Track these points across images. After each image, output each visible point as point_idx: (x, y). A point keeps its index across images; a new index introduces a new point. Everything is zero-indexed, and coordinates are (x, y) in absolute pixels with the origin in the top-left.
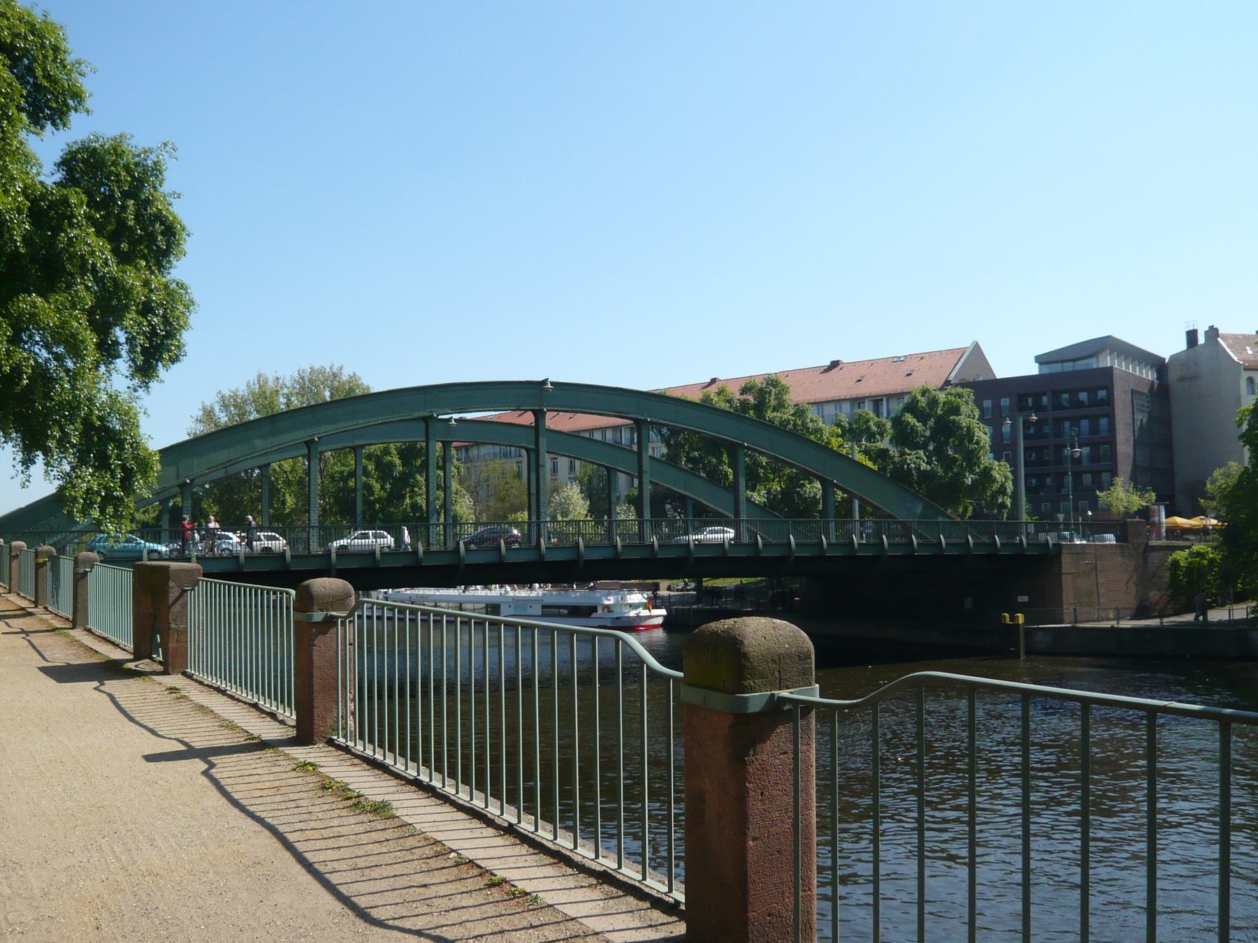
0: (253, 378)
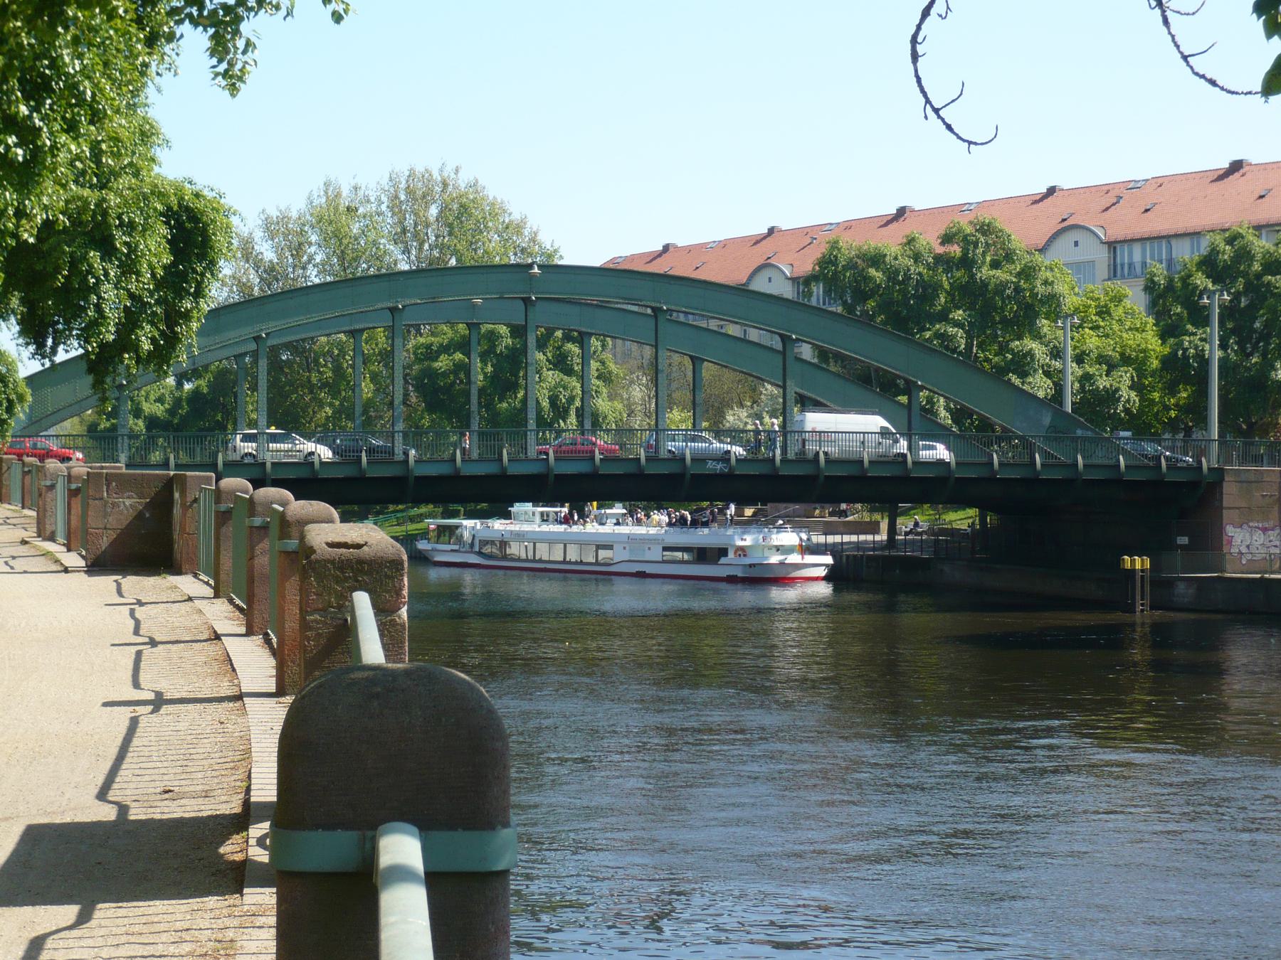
0: (316, 186)
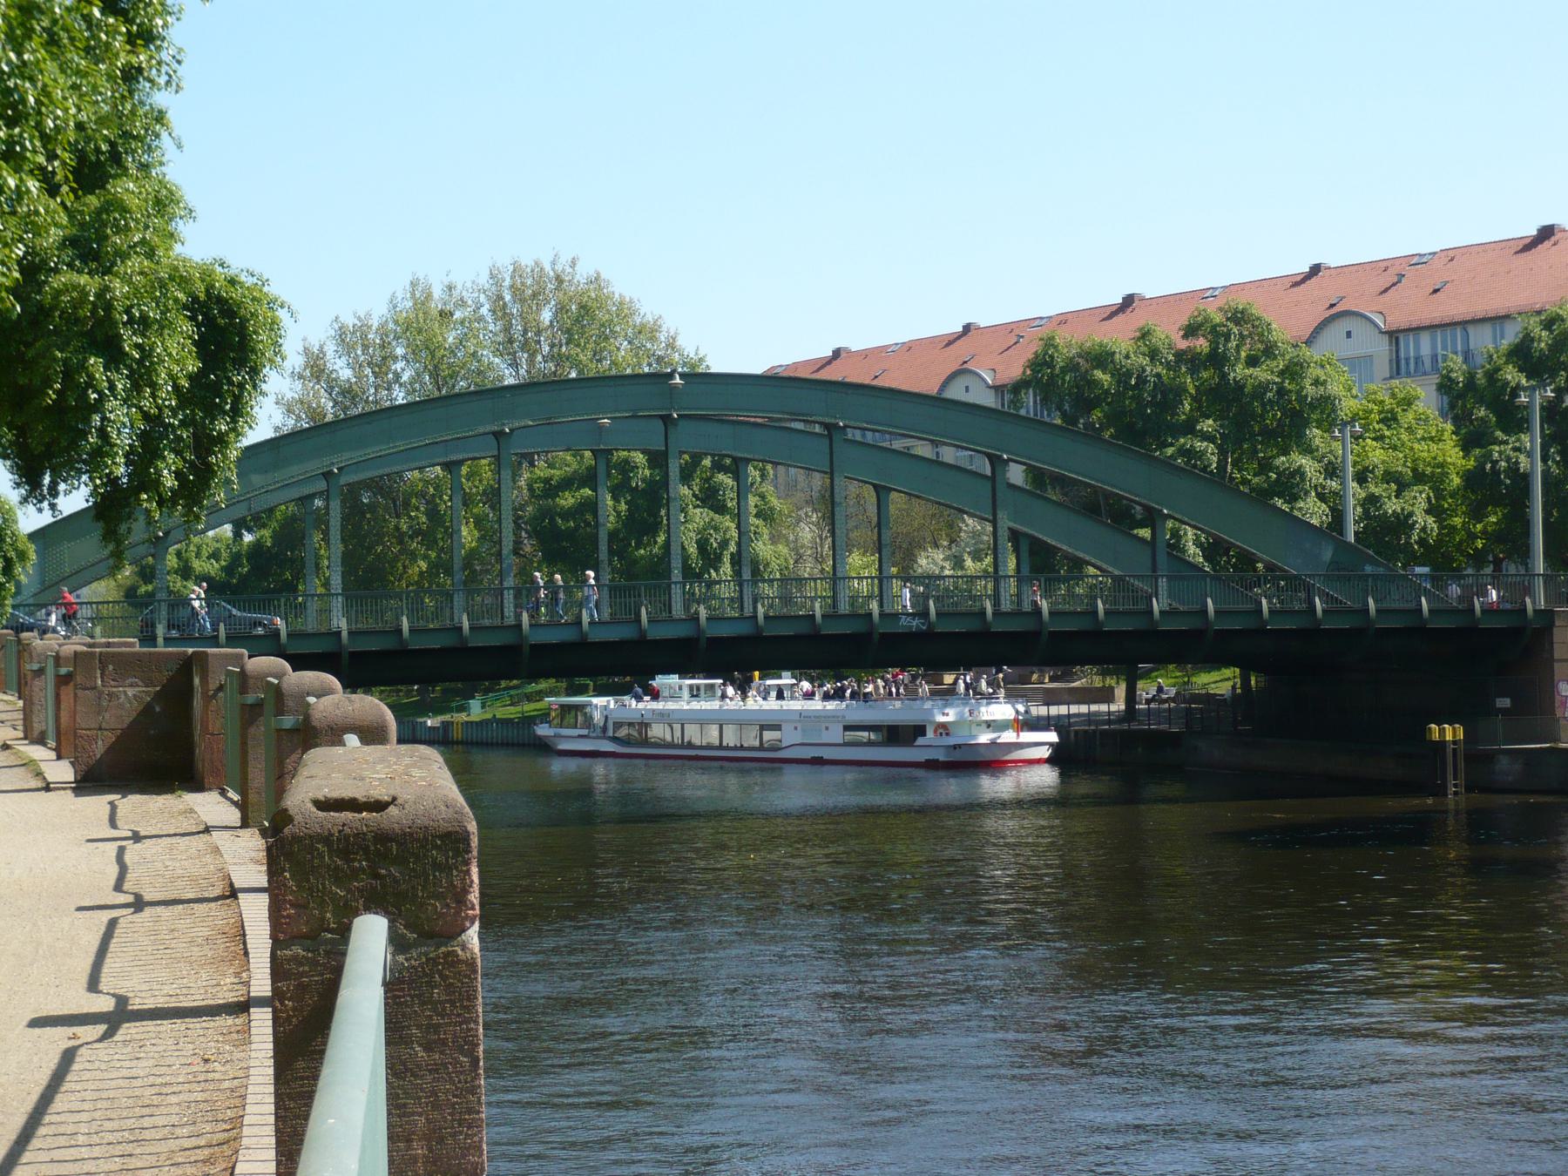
0: (400, 287)
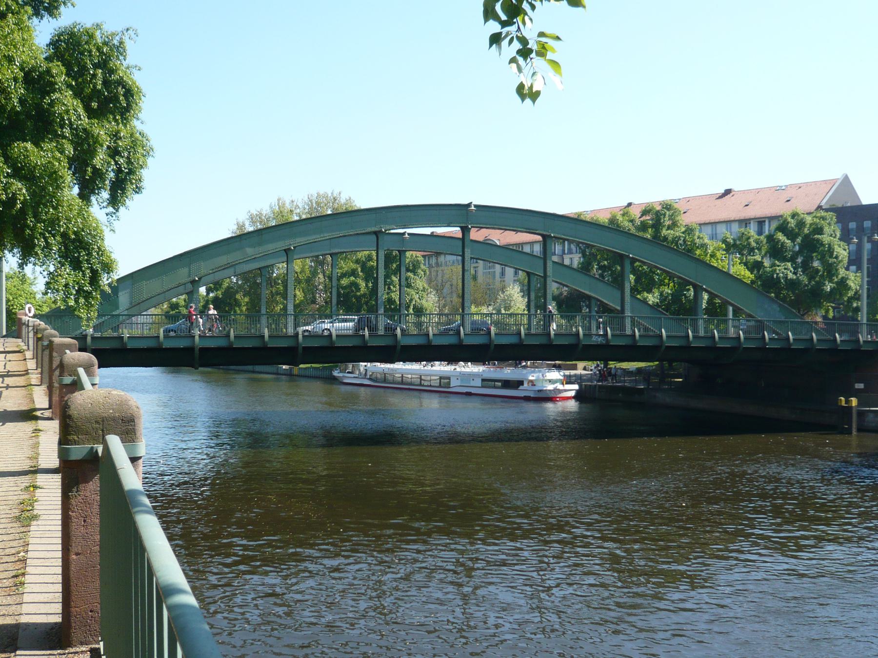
0: (274, 201)
